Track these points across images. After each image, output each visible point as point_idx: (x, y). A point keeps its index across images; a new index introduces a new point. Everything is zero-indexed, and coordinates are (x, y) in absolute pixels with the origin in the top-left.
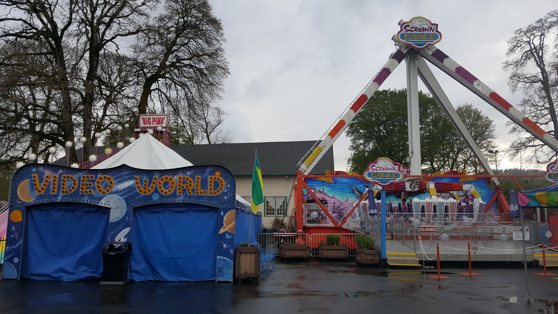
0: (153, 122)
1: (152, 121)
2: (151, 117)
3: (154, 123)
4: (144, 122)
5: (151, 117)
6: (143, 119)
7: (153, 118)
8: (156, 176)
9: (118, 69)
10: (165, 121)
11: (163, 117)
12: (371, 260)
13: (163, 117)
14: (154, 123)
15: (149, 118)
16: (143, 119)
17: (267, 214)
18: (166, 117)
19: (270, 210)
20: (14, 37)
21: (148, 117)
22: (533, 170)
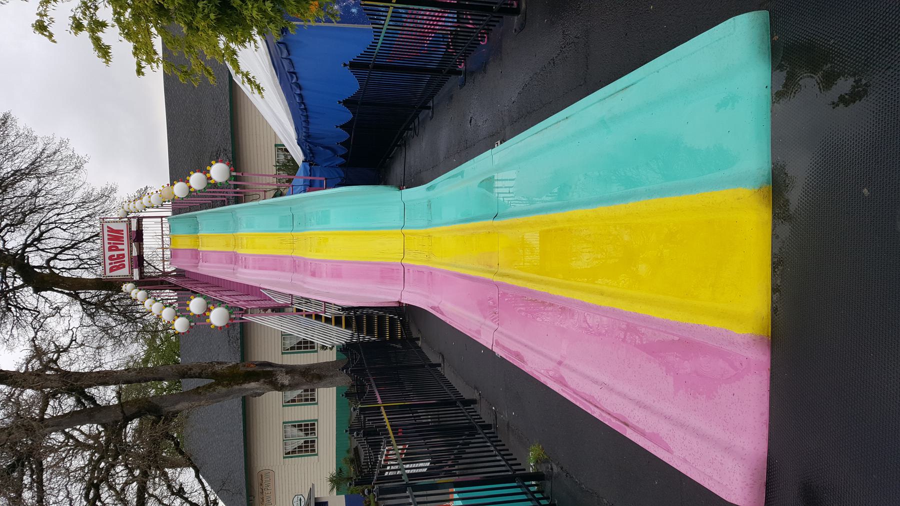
0: (118, 249)
1: (116, 253)
2: (108, 254)
3: (120, 247)
4: (118, 268)
5: (108, 254)
6: (111, 270)
7: (110, 249)
8: (313, 129)
9: (37, 291)
10: (115, 227)
11: (106, 229)
12: (676, 357)
13: (106, 229)
14: (120, 247)
15: (111, 258)
16: (111, 270)
17: (314, 451)
18: (105, 226)
19: (307, 447)
20: (118, 488)
21: (108, 261)
22: (404, 144)
